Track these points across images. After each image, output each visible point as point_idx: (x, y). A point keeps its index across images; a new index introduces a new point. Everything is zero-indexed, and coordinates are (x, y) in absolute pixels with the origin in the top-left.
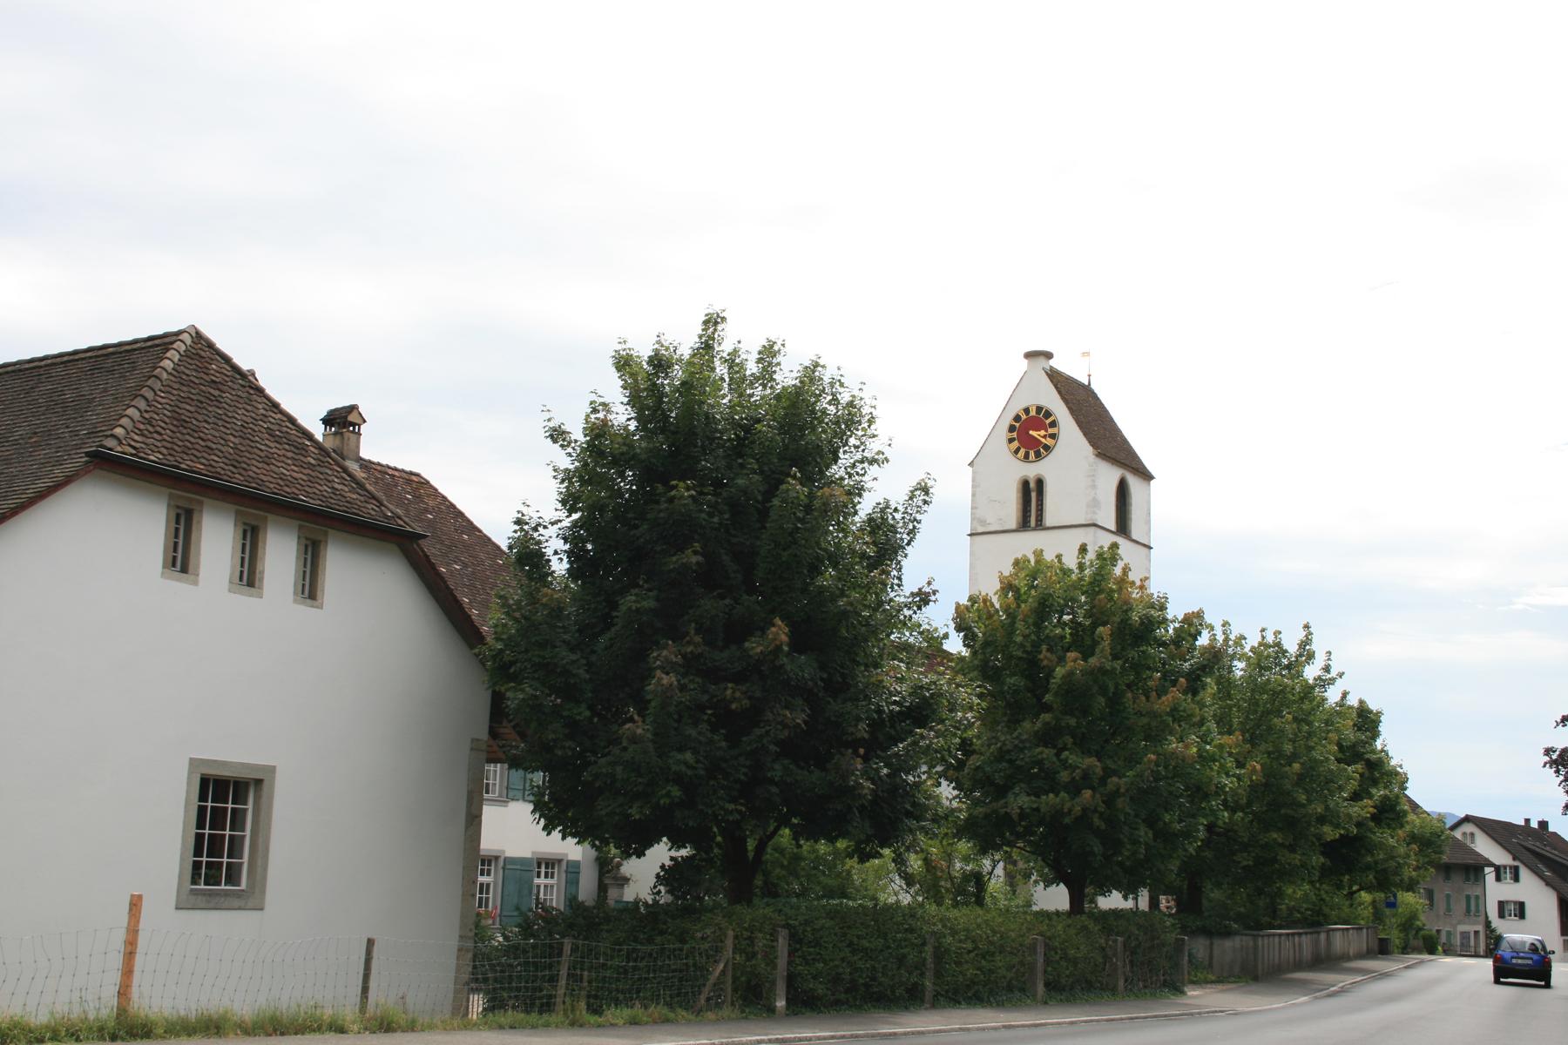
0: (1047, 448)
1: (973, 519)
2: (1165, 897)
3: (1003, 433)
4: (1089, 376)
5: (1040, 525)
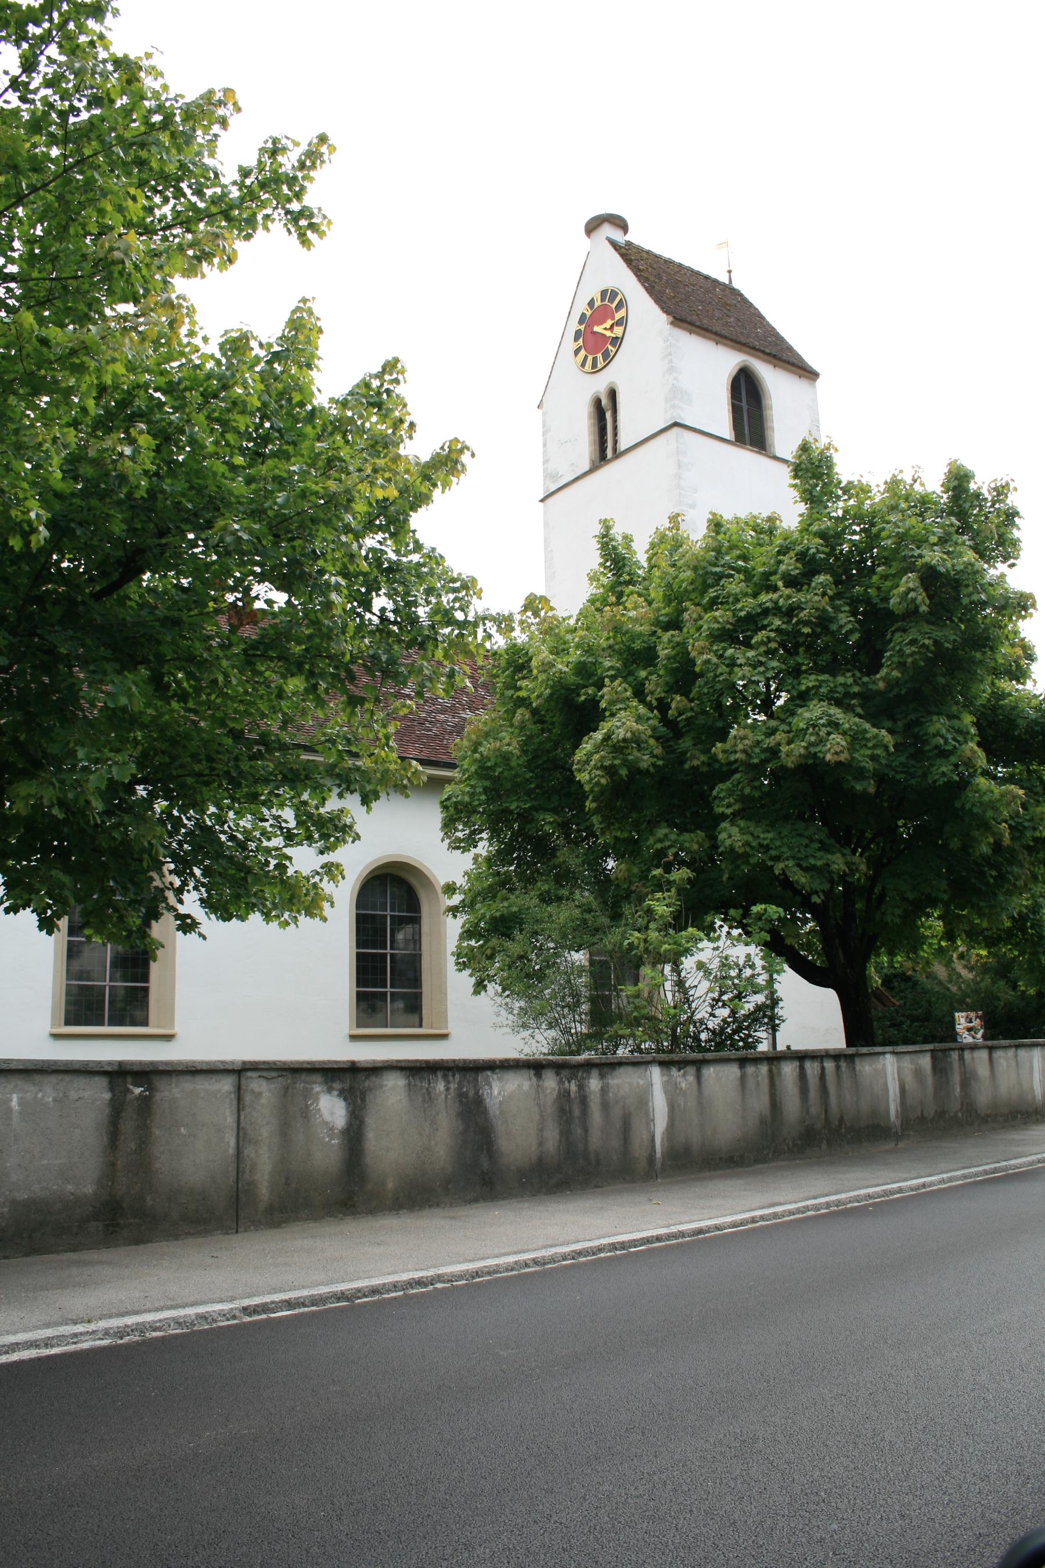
0: (617, 341)
1: (545, 477)
2: (964, 1014)
3: (570, 345)
4: (730, 272)
5: (617, 455)
